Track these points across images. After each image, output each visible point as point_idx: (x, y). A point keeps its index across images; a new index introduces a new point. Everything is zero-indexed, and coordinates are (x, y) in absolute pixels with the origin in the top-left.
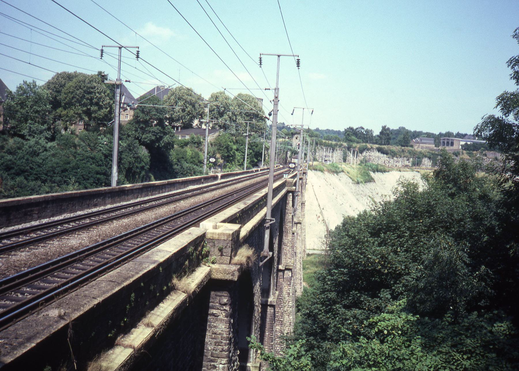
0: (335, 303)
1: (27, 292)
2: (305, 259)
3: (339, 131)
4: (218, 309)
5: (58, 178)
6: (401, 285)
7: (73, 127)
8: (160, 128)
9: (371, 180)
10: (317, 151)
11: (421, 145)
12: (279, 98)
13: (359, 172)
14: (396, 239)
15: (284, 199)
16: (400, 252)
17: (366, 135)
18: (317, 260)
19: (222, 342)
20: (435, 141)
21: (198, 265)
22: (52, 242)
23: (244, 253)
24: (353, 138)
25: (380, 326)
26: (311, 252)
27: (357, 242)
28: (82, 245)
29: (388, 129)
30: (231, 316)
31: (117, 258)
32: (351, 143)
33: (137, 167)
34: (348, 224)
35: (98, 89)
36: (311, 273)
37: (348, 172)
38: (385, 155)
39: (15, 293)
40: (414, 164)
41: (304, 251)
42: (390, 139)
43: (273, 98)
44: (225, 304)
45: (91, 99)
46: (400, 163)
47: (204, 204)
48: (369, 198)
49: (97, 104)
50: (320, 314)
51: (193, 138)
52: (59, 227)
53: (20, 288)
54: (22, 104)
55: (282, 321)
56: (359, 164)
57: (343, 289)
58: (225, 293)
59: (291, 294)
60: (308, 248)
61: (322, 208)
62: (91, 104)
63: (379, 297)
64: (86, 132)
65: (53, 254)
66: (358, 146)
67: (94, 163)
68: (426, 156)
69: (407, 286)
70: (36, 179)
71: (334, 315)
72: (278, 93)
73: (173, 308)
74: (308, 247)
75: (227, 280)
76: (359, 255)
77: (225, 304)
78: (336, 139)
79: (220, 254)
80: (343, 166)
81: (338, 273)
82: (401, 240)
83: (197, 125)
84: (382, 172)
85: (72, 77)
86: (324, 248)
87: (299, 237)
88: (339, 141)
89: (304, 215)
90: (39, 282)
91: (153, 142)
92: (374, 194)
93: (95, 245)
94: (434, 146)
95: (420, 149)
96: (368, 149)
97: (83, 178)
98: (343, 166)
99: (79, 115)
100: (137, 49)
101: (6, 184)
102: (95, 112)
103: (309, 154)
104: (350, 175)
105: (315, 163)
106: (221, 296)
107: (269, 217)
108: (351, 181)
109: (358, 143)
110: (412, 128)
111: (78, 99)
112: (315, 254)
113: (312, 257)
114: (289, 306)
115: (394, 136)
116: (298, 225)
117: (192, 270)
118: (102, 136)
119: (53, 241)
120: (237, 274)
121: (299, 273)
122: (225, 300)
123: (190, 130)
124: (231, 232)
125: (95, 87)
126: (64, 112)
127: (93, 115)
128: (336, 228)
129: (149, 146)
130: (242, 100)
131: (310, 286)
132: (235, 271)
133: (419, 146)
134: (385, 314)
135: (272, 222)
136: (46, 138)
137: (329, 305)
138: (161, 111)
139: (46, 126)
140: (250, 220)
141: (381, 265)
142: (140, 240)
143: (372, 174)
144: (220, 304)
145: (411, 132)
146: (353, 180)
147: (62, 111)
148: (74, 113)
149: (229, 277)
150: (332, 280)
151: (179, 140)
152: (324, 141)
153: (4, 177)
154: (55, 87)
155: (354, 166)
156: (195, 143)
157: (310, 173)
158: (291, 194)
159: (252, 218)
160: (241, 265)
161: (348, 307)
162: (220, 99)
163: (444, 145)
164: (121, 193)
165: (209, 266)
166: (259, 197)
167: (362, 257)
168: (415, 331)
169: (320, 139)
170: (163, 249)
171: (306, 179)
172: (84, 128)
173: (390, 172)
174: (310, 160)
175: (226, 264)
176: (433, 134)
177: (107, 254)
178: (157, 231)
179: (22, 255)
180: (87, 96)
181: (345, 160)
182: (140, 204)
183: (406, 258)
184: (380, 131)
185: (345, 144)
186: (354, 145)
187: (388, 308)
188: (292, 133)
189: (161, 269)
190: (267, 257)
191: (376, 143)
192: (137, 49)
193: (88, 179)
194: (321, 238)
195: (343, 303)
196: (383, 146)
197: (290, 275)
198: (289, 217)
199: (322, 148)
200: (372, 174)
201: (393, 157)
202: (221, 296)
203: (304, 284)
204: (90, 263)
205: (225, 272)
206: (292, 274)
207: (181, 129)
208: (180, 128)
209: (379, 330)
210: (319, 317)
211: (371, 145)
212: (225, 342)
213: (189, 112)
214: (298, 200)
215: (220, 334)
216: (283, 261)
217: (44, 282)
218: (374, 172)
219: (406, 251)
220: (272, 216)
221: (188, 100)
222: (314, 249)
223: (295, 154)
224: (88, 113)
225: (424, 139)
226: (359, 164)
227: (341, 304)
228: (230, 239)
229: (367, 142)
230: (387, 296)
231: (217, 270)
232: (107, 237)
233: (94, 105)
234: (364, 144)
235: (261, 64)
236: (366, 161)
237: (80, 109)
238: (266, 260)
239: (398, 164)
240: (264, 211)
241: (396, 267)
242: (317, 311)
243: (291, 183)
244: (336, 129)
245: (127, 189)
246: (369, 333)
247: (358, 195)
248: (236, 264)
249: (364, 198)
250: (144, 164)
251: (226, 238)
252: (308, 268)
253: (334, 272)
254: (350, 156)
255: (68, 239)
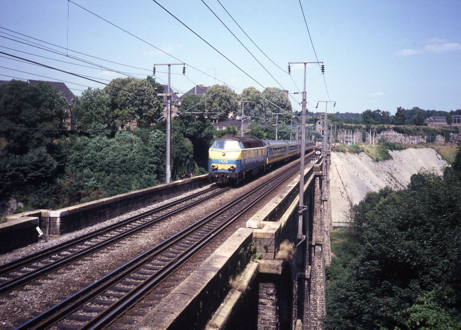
0: (367, 290)
1: (111, 295)
2: (332, 231)
3: (358, 114)
4: (266, 298)
5: (118, 169)
6: (429, 276)
7: (128, 124)
8: (201, 122)
9: (388, 157)
10: (339, 133)
11: (434, 123)
12: (307, 100)
13: (378, 151)
14: (422, 233)
15: (313, 184)
16: (426, 244)
17: (383, 116)
18: (343, 232)
19: (270, 327)
20: (447, 119)
21: (248, 262)
22: (124, 242)
23: (286, 248)
24: (371, 120)
25: (413, 318)
26: (336, 225)
27: (388, 237)
28: (149, 244)
29: (403, 110)
30: (276, 304)
31: (180, 257)
32: (369, 125)
33: (183, 157)
34: (371, 199)
35: (147, 91)
36: (338, 244)
37: (368, 152)
38: (401, 134)
39: (102, 296)
40: (428, 141)
41: (331, 224)
42: (405, 119)
43: (301, 100)
44: (272, 295)
45: (142, 100)
46: (416, 140)
47: (245, 195)
48: (388, 174)
49: (148, 104)
50: (355, 301)
51: (229, 129)
52: (128, 226)
53: (105, 292)
54: (86, 107)
55: (315, 291)
56: (378, 144)
57: (375, 279)
58: (271, 285)
59: (322, 266)
60: (334, 221)
61: (345, 185)
62: (142, 105)
63: (409, 287)
64: (139, 129)
65: (127, 254)
66: (376, 127)
67: (147, 154)
68: (439, 134)
69: (435, 277)
70: (101, 170)
71: (368, 302)
72: (305, 96)
73: (231, 308)
74: (334, 221)
75: (272, 273)
76: (389, 249)
77: (272, 295)
78: (356, 122)
79: (265, 251)
80: (364, 146)
81: (370, 265)
82: (427, 234)
83: (232, 117)
84: (399, 150)
85: (126, 83)
86: (348, 221)
87: (325, 213)
88: (358, 123)
89: (329, 192)
90: (120, 284)
91: (195, 135)
92: (393, 169)
93: (160, 244)
94: (446, 123)
95: (433, 127)
96: (385, 130)
97: (139, 167)
98: (364, 146)
99: (133, 114)
100: (183, 66)
101: (75, 176)
102: (146, 111)
103: (331, 136)
104: (369, 154)
105: (338, 144)
106: (267, 287)
107: (301, 205)
108: (370, 159)
109: (375, 124)
110: (425, 107)
111: (130, 101)
112: (340, 227)
113: (338, 229)
114: (320, 276)
115: (409, 116)
116: (325, 202)
117: (243, 267)
118: (153, 132)
119: (125, 240)
120: (280, 268)
121: (328, 247)
122: (272, 291)
123: (225, 122)
124: (274, 232)
125: (145, 90)
126: (120, 113)
127: (144, 114)
128: (360, 203)
129: (191, 138)
130: (269, 93)
131: (337, 256)
132: (279, 266)
133: (432, 124)
134: (417, 306)
135: (304, 209)
136: (107, 135)
137: (363, 293)
138: (201, 107)
139: (106, 125)
140: (286, 210)
141: (411, 258)
142: (195, 236)
143: (390, 152)
144: (267, 294)
145: (424, 111)
146: (372, 159)
147: (118, 112)
148: (128, 113)
149: (274, 271)
150: (364, 270)
151: (217, 132)
152: (344, 124)
153: (74, 170)
154: (112, 91)
155: (373, 145)
156: (231, 133)
157: (333, 154)
158: (318, 178)
159: (288, 208)
160: (284, 259)
161: (381, 295)
162: (251, 94)
163: (455, 122)
164: (174, 190)
165: (257, 262)
166: (293, 188)
167: (392, 250)
168: (445, 322)
169: (342, 123)
170: (220, 255)
171: (330, 161)
172: (137, 125)
173: (407, 150)
174: (333, 142)
175: (270, 259)
176: (445, 112)
177: (171, 253)
178: (209, 226)
179: (102, 258)
180: (138, 98)
181: (364, 140)
182: (191, 198)
183: (432, 251)
184: (396, 112)
185: (364, 126)
186: (373, 126)
187: (419, 299)
188: (314, 119)
189: (220, 275)
190: (301, 240)
191: (392, 123)
192: (183, 66)
193: (143, 169)
194: (346, 213)
195: (376, 291)
196: (399, 126)
197: (321, 250)
198: (317, 198)
199: (343, 131)
200: (390, 152)
201: (409, 135)
202: (267, 287)
203: (332, 254)
204: (158, 263)
205: (270, 266)
206: (322, 249)
207: (218, 121)
208: (217, 121)
209: (412, 321)
210: (355, 303)
211: (388, 125)
212: (272, 327)
213: (224, 106)
214: (324, 183)
215: (268, 320)
216: (314, 237)
217: (123, 284)
218: (392, 150)
219: (434, 244)
220: (304, 204)
221: (223, 96)
222: (339, 222)
223: (319, 137)
224: (140, 112)
225: (437, 118)
226: (378, 144)
227: (374, 292)
228: (274, 238)
229: (384, 123)
230: (416, 287)
231: (264, 265)
232: (169, 234)
233: (145, 105)
234: (382, 125)
235: (290, 72)
236: (384, 141)
237: (133, 109)
238: (300, 242)
239: (413, 142)
240: (298, 199)
241: (424, 260)
242: (352, 297)
243: (318, 168)
244: (354, 112)
245: (179, 184)
246: (401, 320)
247: (378, 171)
248: (279, 259)
249: (384, 174)
250: (188, 154)
251: (270, 237)
252: (335, 240)
253: (367, 264)
254: (369, 137)
255: (137, 238)
